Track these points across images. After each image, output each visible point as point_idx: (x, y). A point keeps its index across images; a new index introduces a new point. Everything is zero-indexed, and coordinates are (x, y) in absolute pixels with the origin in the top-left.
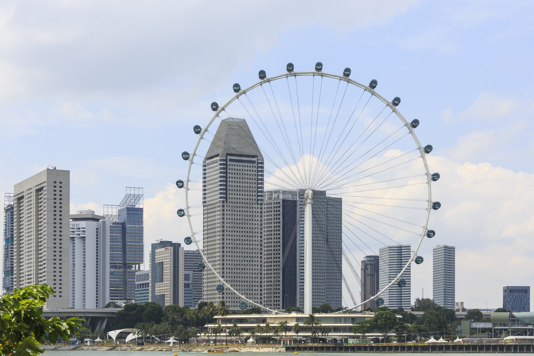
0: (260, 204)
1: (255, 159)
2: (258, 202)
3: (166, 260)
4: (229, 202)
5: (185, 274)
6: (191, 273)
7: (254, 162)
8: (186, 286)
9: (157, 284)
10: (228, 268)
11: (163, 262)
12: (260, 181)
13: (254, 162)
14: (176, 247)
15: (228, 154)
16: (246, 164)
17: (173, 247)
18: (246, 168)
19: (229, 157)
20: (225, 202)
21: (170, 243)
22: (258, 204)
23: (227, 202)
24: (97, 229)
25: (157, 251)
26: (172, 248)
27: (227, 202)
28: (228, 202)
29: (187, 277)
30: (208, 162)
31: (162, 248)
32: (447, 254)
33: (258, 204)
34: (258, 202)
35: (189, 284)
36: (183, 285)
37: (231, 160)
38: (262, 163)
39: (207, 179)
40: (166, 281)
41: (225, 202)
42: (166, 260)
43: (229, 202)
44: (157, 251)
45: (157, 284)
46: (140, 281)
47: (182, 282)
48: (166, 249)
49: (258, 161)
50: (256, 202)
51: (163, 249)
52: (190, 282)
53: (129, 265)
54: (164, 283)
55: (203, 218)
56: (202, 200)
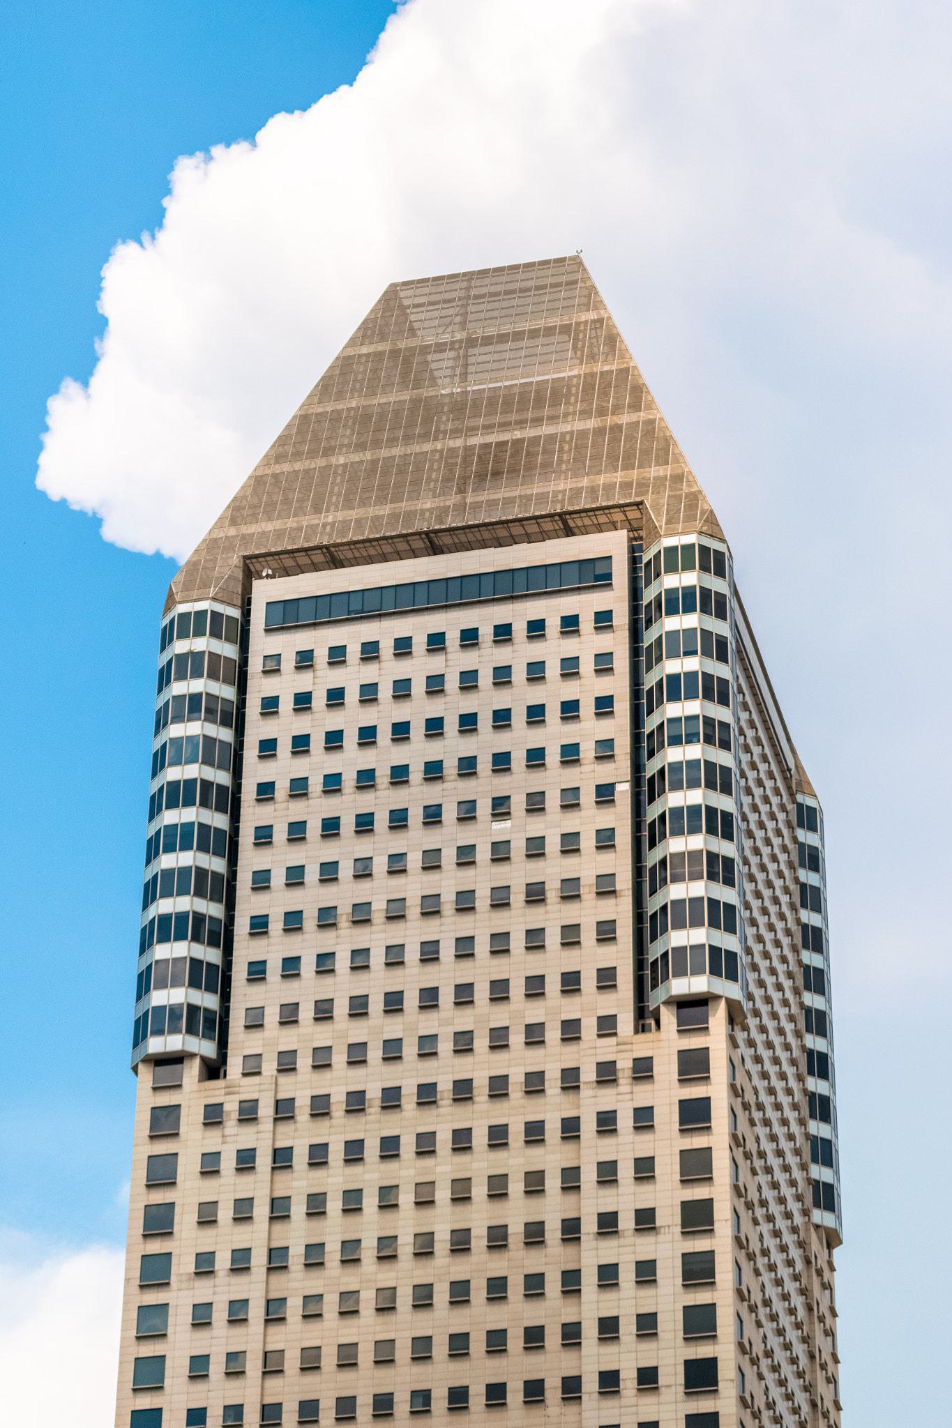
19: (267, 591)
27: (213, 1070)
50: (621, 1003)
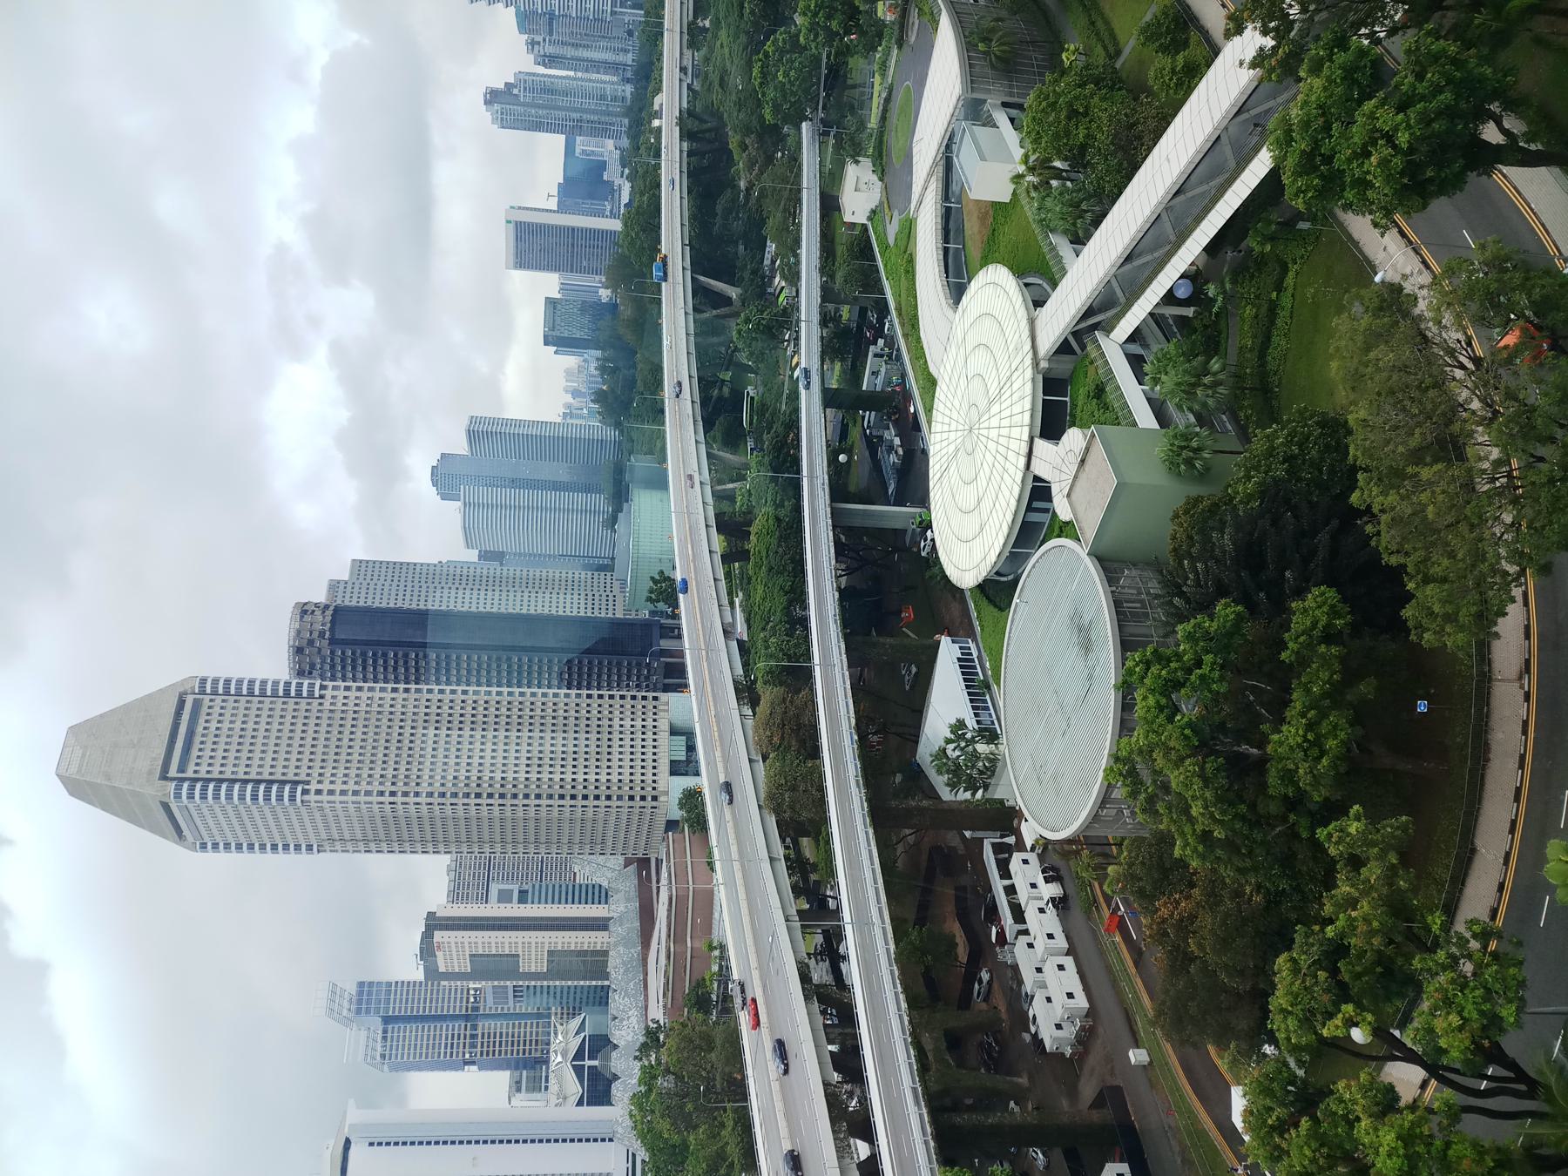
0: (323, 692)
1: (189, 700)
2: (317, 695)
3: (467, 949)
4: (308, 775)
5: (499, 902)
6: (495, 888)
7: (197, 705)
8: (523, 897)
9: (523, 967)
10: (576, 742)
11: (471, 956)
12: (252, 691)
13: (197, 705)
14: (434, 923)
15: (164, 777)
16: (201, 723)
17: (435, 932)
18: (213, 725)
19: (173, 772)
20: (306, 787)
21: (427, 936)
22: (321, 697)
23: (308, 783)
24: (371, 1144)
25: (442, 969)
26: (438, 936)
27: (308, 783)
28: (309, 779)
29: (504, 897)
30: (190, 838)
31: (435, 956)
32: (423, 996)
33: (321, 697)
34: (317, 695)
35: (520, 892)
36: (522, 906)
37: (181, 769)
38: (203, 681)
39: (218, 839)
40: (516, 947)
41: (306, 787)
42: (467, 949)
43: (308, 775)
44: (442, 969)
45: (523, 967)
46: (507, 998)
47: (515, 910)
48: (439, 947)
49: (197, 691)
51: (439, 954)
52: (515, 888)
53: (469, 1010)
54: (520, 953)
55: (436, 856)
56: (304, 857)
